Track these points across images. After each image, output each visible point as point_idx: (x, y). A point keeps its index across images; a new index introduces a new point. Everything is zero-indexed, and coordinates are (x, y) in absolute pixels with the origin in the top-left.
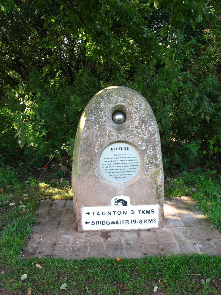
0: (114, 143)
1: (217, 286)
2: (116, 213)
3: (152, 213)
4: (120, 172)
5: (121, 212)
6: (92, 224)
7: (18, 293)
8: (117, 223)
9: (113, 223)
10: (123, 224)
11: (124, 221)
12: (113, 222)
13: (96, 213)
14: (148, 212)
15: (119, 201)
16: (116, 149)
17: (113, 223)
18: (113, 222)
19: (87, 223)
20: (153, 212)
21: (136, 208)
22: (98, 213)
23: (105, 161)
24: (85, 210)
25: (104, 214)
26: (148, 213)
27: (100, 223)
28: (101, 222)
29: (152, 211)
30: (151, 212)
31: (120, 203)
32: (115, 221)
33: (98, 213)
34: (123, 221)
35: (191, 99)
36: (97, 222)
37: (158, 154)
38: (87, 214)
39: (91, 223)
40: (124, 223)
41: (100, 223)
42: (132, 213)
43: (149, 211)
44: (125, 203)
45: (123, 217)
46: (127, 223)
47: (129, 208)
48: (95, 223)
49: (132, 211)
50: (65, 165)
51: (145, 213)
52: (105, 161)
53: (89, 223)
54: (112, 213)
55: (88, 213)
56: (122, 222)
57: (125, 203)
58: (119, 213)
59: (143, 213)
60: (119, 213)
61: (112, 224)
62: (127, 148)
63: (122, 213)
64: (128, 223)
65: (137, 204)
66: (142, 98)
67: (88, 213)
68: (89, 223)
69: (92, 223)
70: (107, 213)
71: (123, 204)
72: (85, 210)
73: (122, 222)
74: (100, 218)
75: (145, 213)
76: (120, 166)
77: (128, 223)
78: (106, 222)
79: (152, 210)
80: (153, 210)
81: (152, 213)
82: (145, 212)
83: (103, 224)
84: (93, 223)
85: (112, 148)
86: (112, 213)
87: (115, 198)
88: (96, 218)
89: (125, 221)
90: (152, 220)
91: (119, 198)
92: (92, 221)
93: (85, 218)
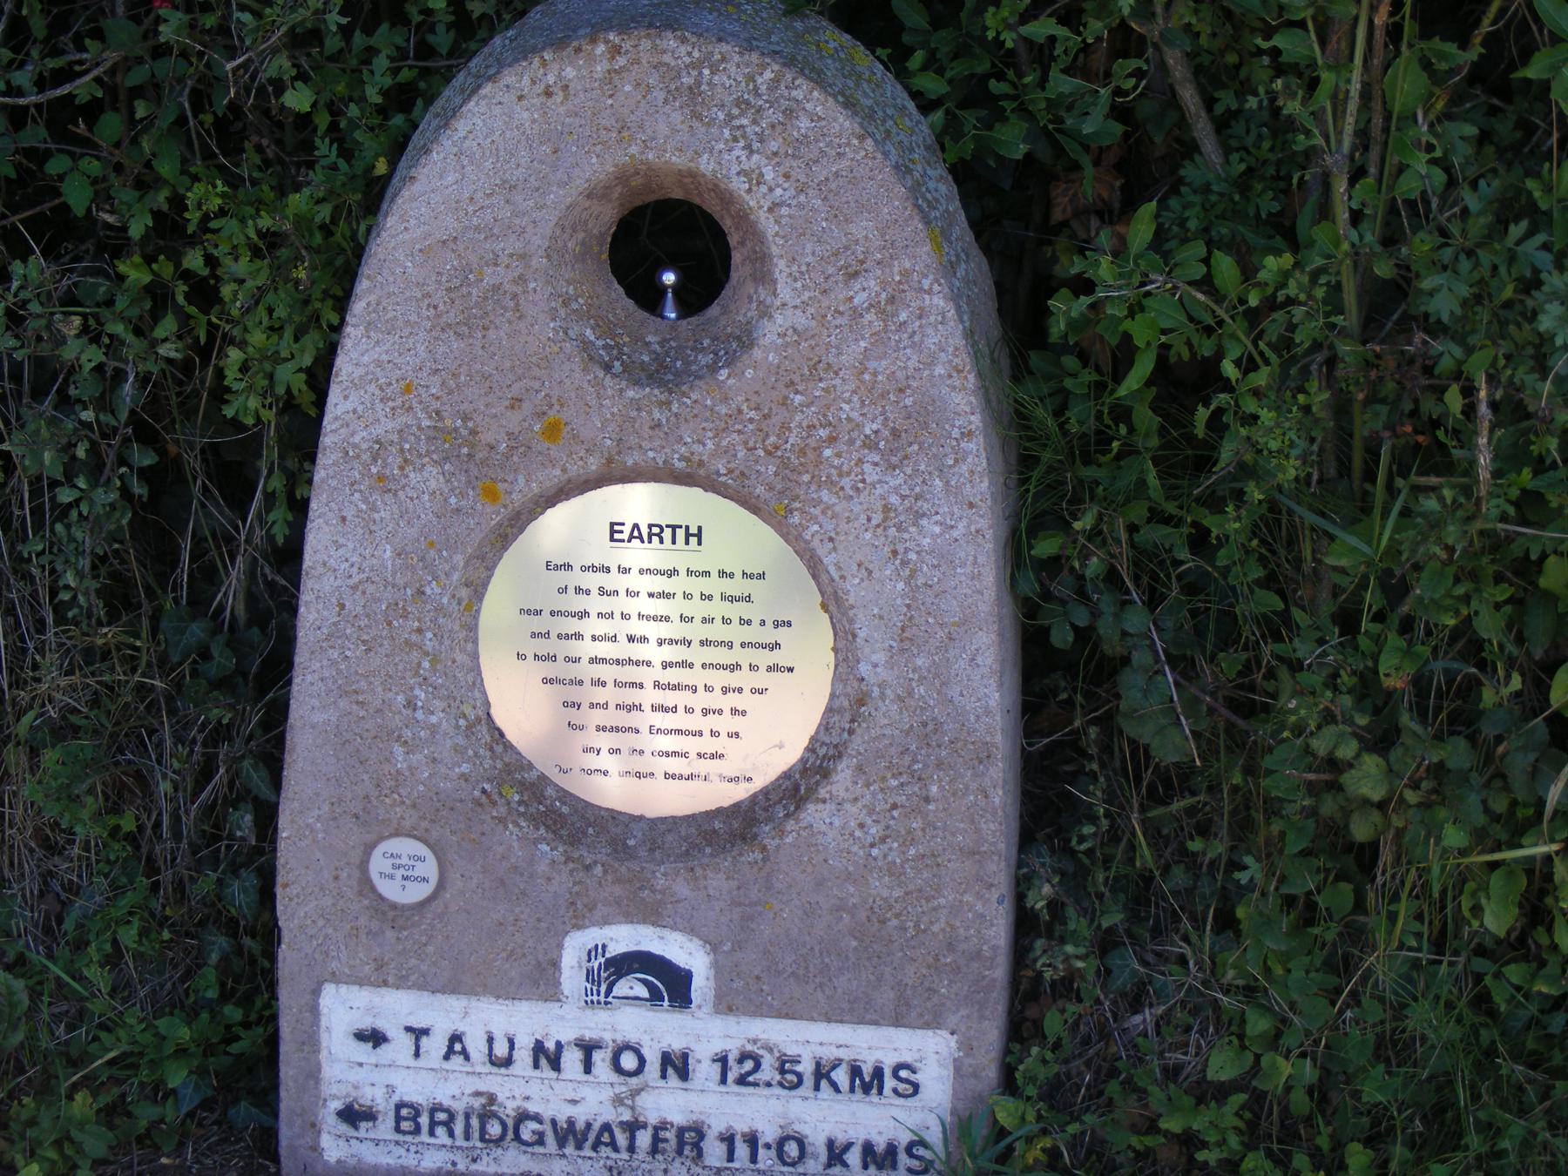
2: (601, 1059)
6: (612, 539)
8: (606, 1138)
11: (662, 1134)
13: (435, 1045)
14: (868, 1081)
15: (623, 965)
19: (353, 1115)
25: (501, 1050)
26: (866, 1089)
29: (895, 1075)
30: (889, 1083)
31: (630, 986)
33: (456, 1038)
41: (459, 1128)
43: (878, 1073)
48: (424, 1120)
50: (889, 146)
51: (837, 1090)
55: (375, 1038)
59: (824, 1083)
64: (700, 543)
66: (392, 201)
67: (375, 1038)
69: (399, 1118)
70: (523, 1056)
75: (837, 1090)
76: (646, 577)
77: (700, 543)
78: (510, 1135)
79: (903, 1074)
86: (572, 1060)
90: (878, 1073)
91: (623, 938)
92: (612, 524)
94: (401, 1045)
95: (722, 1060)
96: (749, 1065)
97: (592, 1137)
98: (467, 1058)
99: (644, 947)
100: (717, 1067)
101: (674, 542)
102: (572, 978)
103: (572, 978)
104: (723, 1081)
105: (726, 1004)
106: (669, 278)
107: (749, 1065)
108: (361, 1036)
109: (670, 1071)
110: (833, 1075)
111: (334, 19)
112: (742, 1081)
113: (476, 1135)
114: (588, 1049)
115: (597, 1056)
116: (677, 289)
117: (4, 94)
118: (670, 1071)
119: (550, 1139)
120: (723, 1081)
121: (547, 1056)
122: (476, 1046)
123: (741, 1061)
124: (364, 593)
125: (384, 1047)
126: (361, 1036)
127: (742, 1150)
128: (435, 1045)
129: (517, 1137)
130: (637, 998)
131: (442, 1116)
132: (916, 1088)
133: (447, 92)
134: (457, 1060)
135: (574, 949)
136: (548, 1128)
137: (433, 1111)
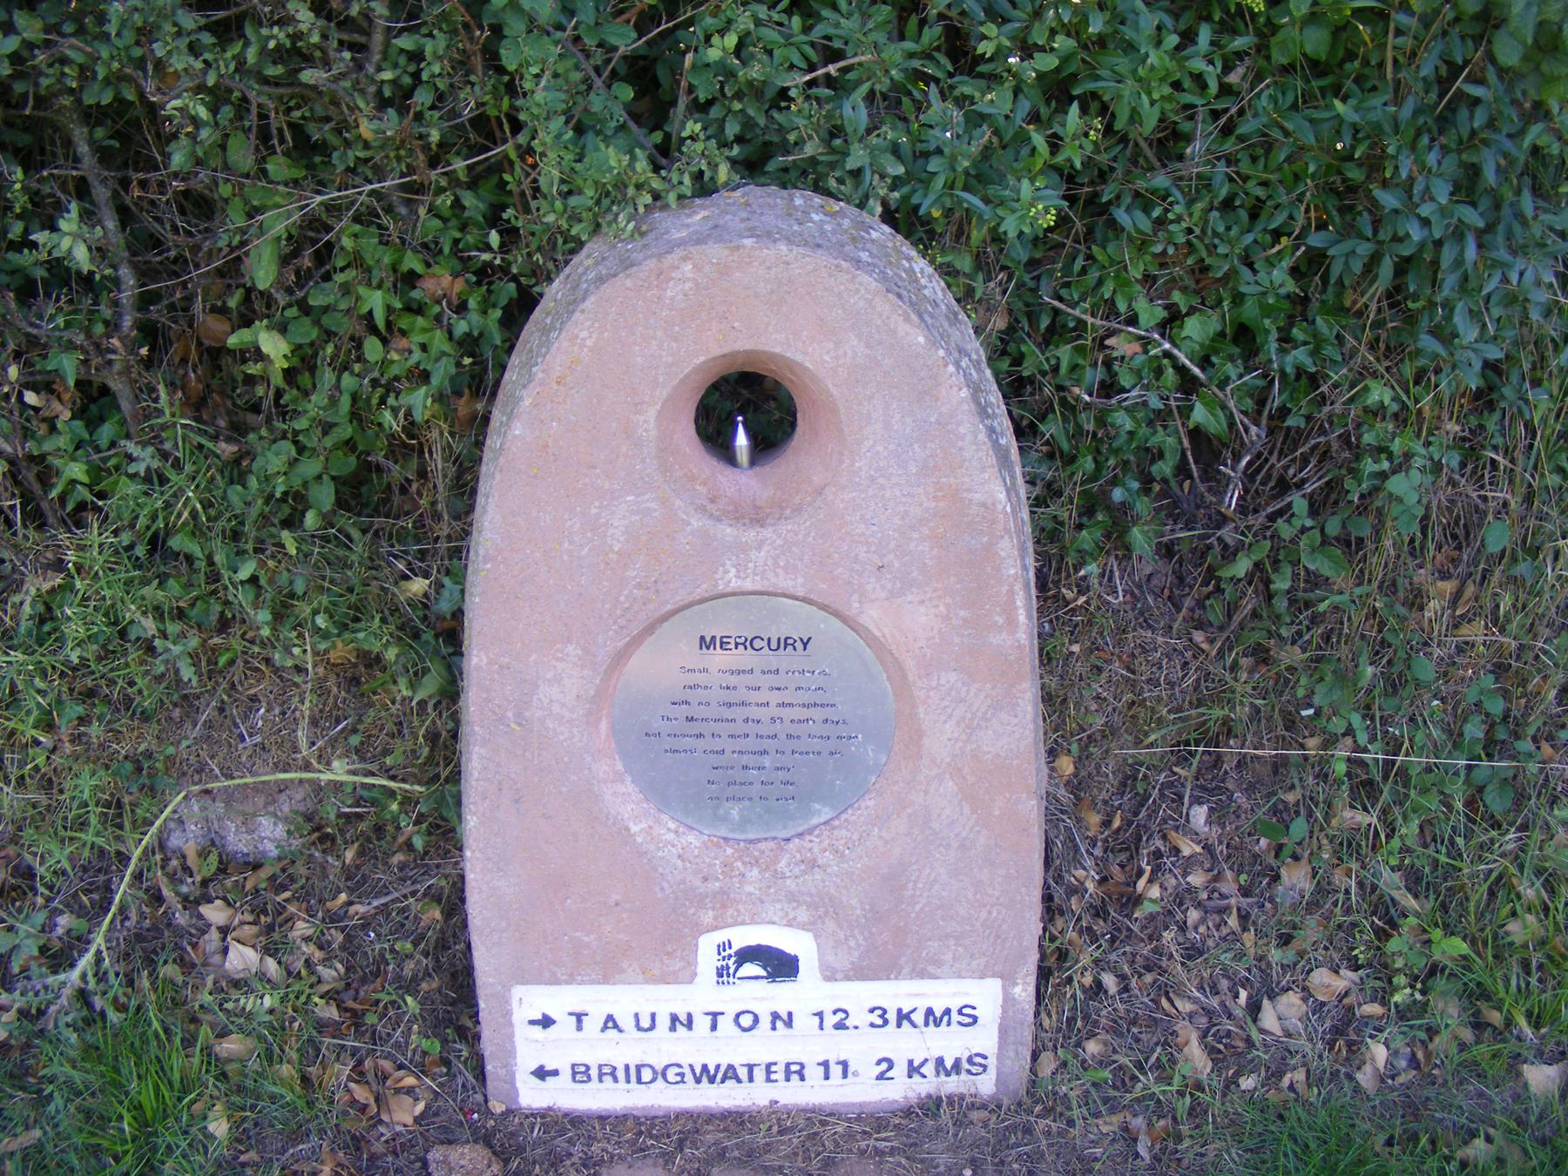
1: (361, 727)
2: (725, 1023)
3: (960, 1023)
5: (756, 1019)
7: (1560, 470)
10: (768, 1080)
12: (705, 1068)
13: (593, 1024)
15: (748, 954)
16: (732, 646)
17: (706, 1075)
18: (705, 1068)
19: (541, 1073)
20: (967, 1020)
21: (860, 996)
22: (610, 1018)
24: (530, 1000)
25: (646, 1023)
27: (621, 1074)
28: (627, 1067)
29: (960, 1012)
30: (955, 1017)
31: (750, 969)
32: (718, 1067)
33: (610, 1018)
34: (768, 1066)
36: (608, 1072)
38: (538, 1028)
39: (566, 1073)
40: (773, 1077)
41: (621, 1074)
42: (879, 1021)
44: (781, 966)
45: (763, 1047)
46: (795, 1077)
49: (879, 1012)
53: (555, 1073)
55: (546, 1022)
56: (759, 1074)
57: (781, 966)
58: (747, 1022)
60: (747, 1022)
61: (698, 1081)
63: (765, 1021)
65: (859, 973)
67: (546, 1022)
68: (555, 1073)
69: (574, 1074)
72: (530, 1000)
73: (759, 1074)
74: (624, 1050)
75: (914, 1026)
81: (960, 1023)
82: (918, 1018)
83: (639, 1081)
84: (580, 1073)
85: (702, 638)
86: (702, 1023)
87: (720, 936)
88: (597, 1049)
89: (780, 1068)
90: (948, 1012)
91: (744, 936)
93: (530, 1049)
94: (565, 1025)
97: (720, 1076)
99: (764, 942)
101: (628, 1081)
102: (707, 958)
103: (707, 958)
110: (912, 1016)
111: (380, 9)
112: (840, 1026)
113: (633, 1078)
114: (715, 1016)
119: (689, 1077)
122: (626, 1022)
123: (835, 1012)
125: (553, 1027)
128: (593, 1024)
129: (655, 1072)
130: (757, 978)
131: (794, 1068)
132: (975, 1019)
135: (707, 947)
136: (687, 1071)
137: (788, 1065)
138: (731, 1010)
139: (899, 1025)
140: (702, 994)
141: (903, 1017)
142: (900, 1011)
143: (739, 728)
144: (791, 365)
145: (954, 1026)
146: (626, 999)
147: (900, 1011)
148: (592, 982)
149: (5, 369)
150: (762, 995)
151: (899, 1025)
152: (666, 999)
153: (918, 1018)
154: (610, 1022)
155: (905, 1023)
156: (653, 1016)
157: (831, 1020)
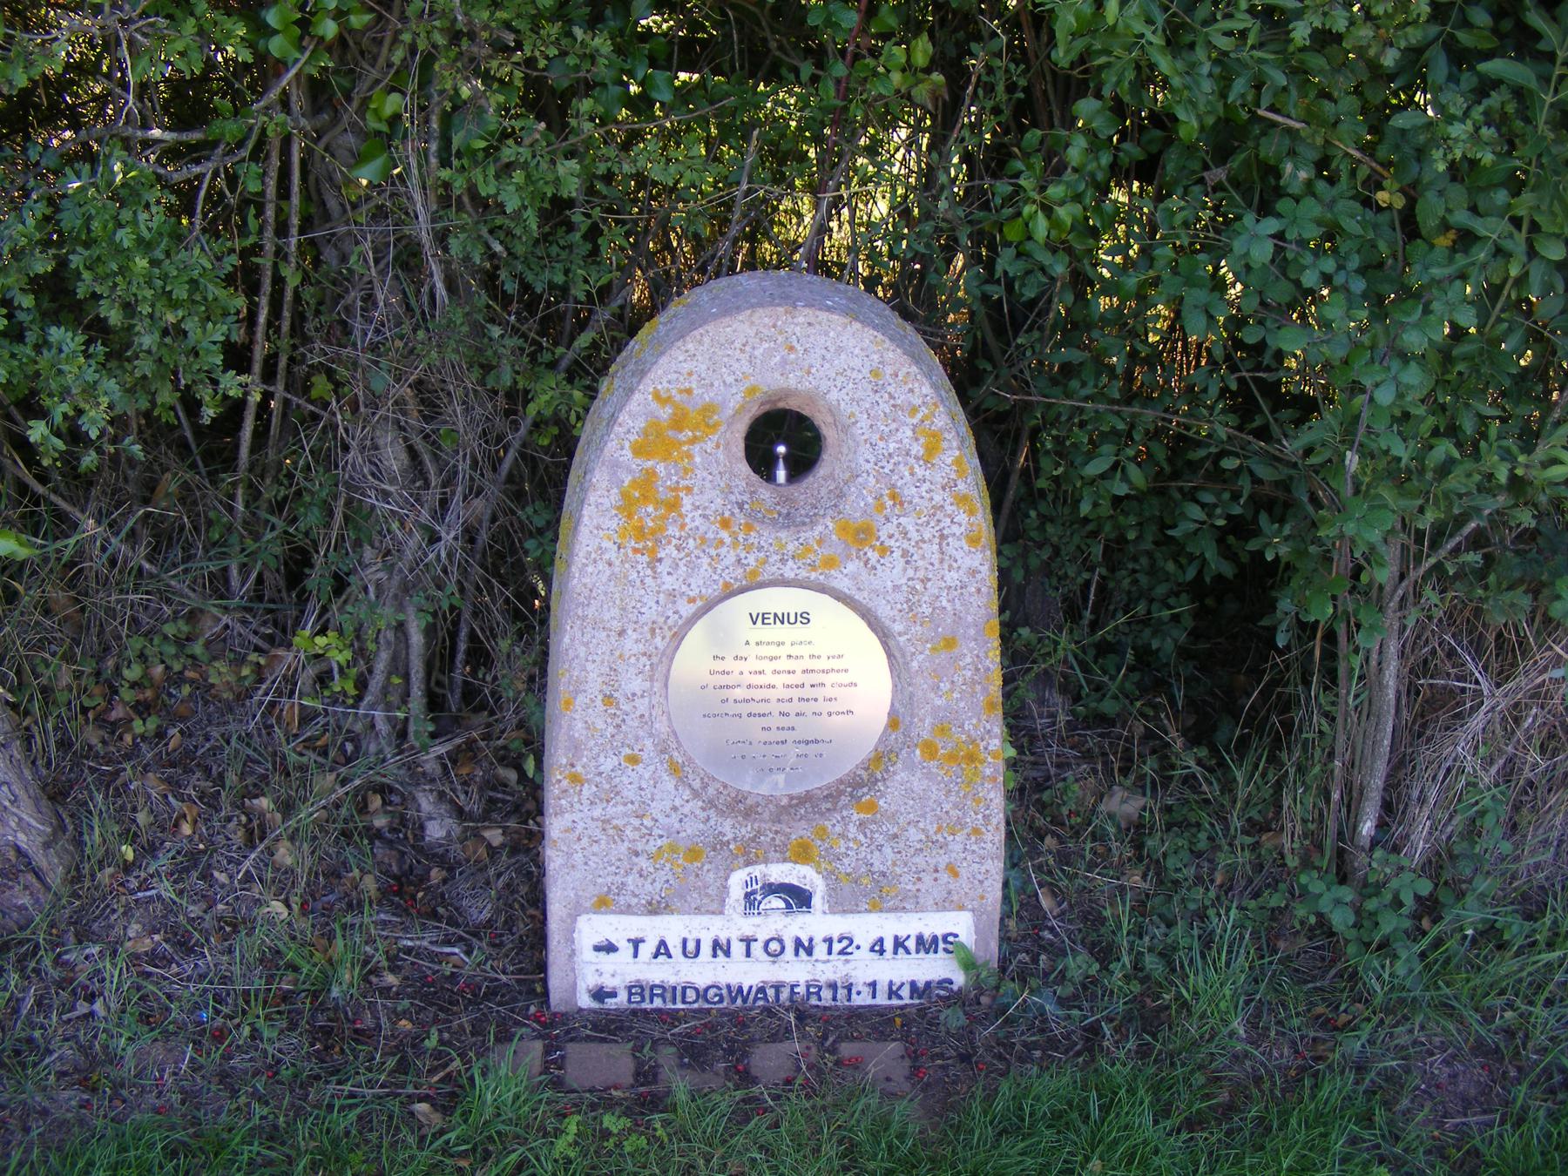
0: (874, 630)
2: (757, 948)
4: (775, 672)
9: (781, 619)
13: (647, 950)
15: (772, 889)
18: (740, 989)
22: (663, 943)
23: (715, 657)
24: (593, 928)
25: (691, 946)
30: (941, 945)
33: (663, 943)
35: (222, 1057)
37: (664, 587)
44: (798, 898)
47: (817, 923)
51: (908, 952)
52: (715, 657)
54: (738, 948)
55: (610, 948)
57: (798, 898)
59: (901, 950)
62: (805, 618)
67: (610, 948)
69: (630, 994)
70: (706, 949)
71: (789, 906)
72: (593, 928)
75: (908, 952)
79: (951, 939)
80: (956, 936)
86: (738, 948)
90: (935, 939)
91: (779, 872)
95: (829, 941)
96: (845, 943)
98: (670, 956)
100: (826, 946)
104: (830, 952)
105: (838, 905)
106: (781, 449)
107: (845, 943)
108: (598, 949)
109: (719, 952)
112: (842, 952)
113: (679, 998)
114: (748, 941)
115: (753, 945)
116: (786, 458)
117: (315, 4)
118: (719, 952)
120: (830, 952)
121: (721, 948)
123: (840, 941)
124: (683, 526)
126: (598, 949)
127: (841, 993)
128: (647, 950)
133: (632, 343)
134: (661, 958)
135: (737, 882)
136: (724, 992)
137: (629, 988)
138: (762, 937)
139: (895, 953)
140: (733, 924)
141: (899, 944)
142: (896, 938)
143: (784, 664)
144: (811, 398)
145: (941, 953)
146: (673, 928)
147: (896, 938)
148: (538, 679)
149: (873, 1175)
150: (775, 921)
151: (895, 953)
152: (705, 928)
153: (911, 944)
154: (662, 949)
155: (901, 950)
156: (698, 942)
157: (837, 947)
